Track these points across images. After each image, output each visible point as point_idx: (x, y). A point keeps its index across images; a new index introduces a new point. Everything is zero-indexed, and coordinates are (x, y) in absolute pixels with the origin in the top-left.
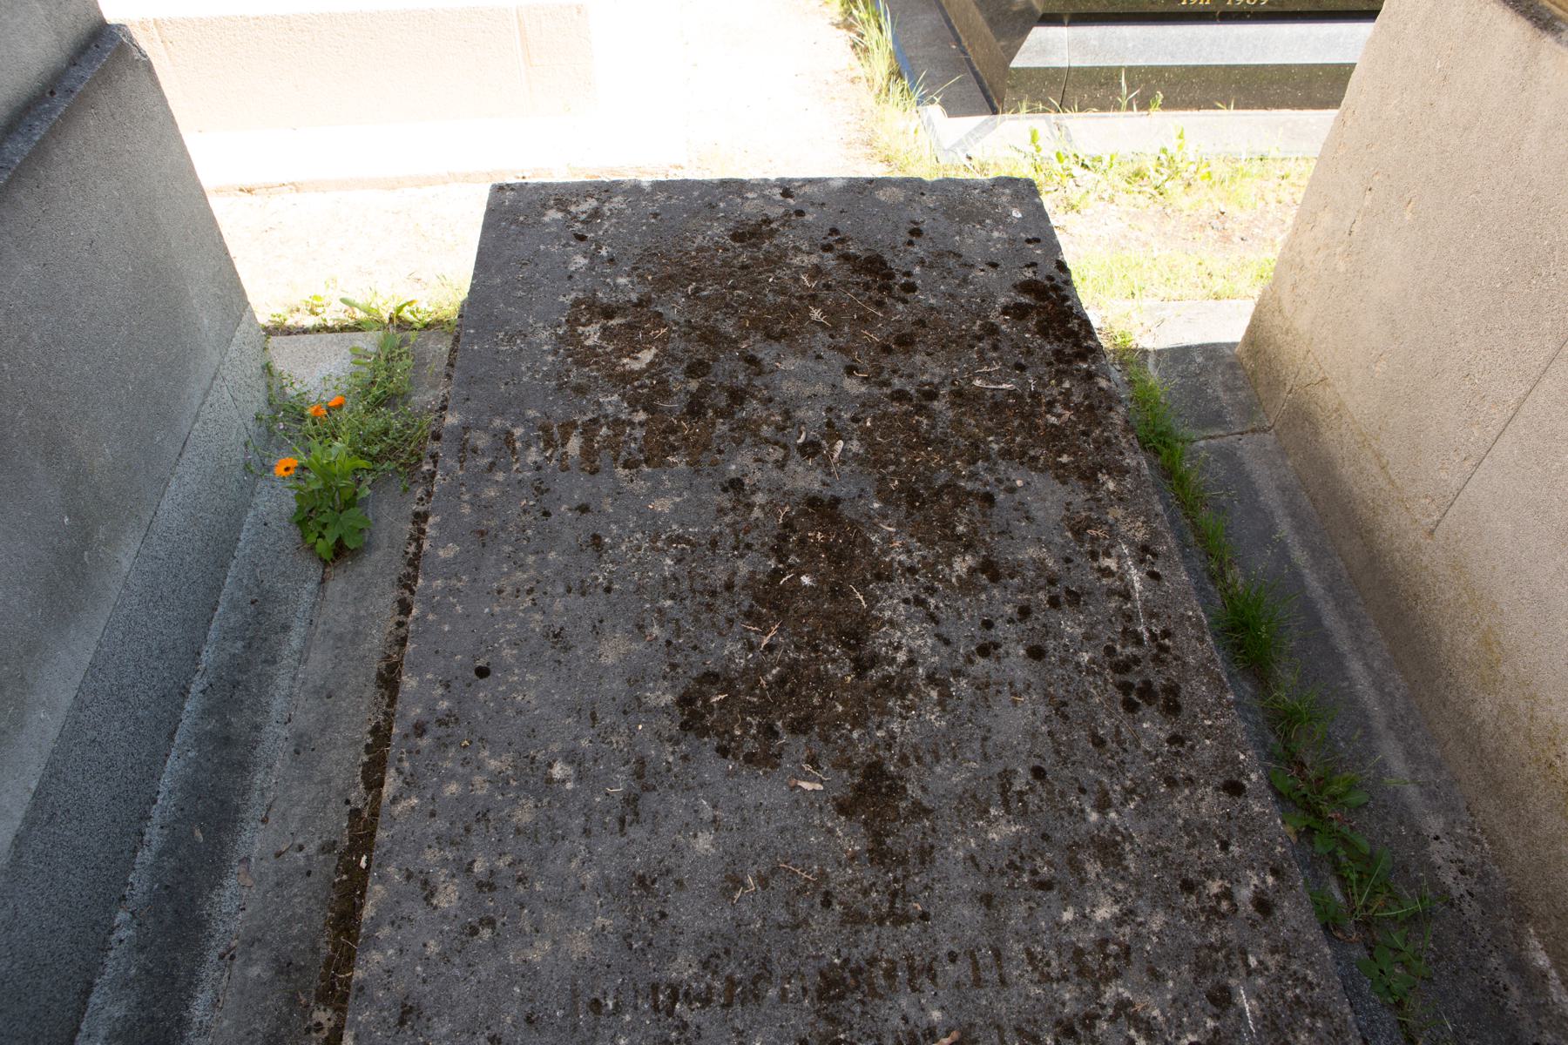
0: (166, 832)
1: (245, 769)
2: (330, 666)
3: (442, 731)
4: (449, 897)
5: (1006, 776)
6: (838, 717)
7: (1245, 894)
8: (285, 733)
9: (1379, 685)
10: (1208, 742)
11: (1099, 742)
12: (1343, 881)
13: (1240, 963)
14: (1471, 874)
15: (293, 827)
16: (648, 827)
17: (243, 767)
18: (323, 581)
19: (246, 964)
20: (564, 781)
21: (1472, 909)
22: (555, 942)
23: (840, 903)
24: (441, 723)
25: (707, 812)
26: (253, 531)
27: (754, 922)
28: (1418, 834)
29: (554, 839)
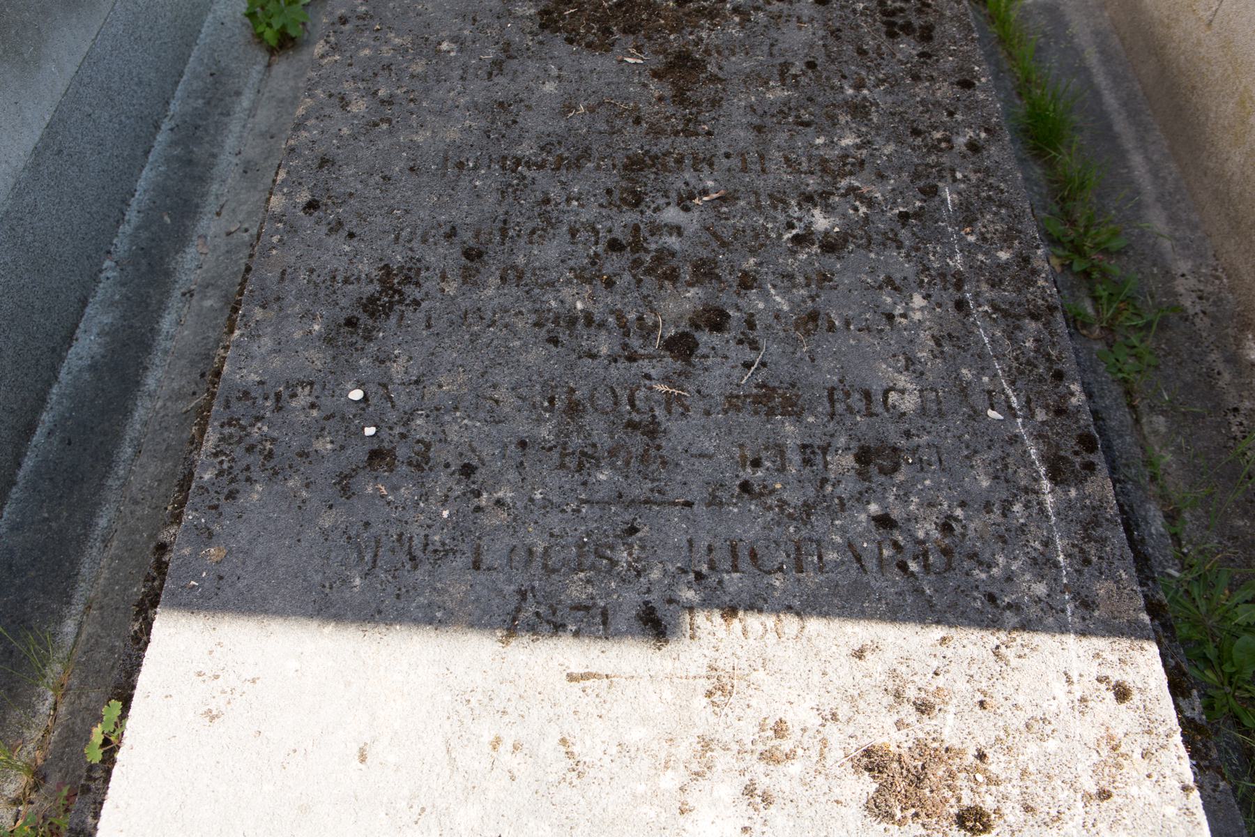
0: (142, 215)
1: (204, 181)
2: (273, 118)
3: (360, 22)
4: (359, 106)
5: (785, 66)
6: (661, 26)
7: (960, 141)
8: (236, 160)
9: (1155, 173)
10: (951, 58)
11: (862, 52)
12: (1096, 300)
13: (949, 176)
14: (1208, 300)
15: (241, 217)
16: (510, 77)
17: (203, 179)
18: (269, 66)
19: (202, 299)
20: (449, 52)
21: (1202, 323)
22: (433, 132)
23: (647, 123)
24: (359, 18)
25: (554, 70)
26: (212, 28)
27: (581, 129)
28: (1167, 272)
29: (438, 81)
